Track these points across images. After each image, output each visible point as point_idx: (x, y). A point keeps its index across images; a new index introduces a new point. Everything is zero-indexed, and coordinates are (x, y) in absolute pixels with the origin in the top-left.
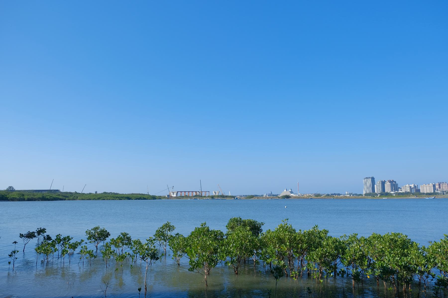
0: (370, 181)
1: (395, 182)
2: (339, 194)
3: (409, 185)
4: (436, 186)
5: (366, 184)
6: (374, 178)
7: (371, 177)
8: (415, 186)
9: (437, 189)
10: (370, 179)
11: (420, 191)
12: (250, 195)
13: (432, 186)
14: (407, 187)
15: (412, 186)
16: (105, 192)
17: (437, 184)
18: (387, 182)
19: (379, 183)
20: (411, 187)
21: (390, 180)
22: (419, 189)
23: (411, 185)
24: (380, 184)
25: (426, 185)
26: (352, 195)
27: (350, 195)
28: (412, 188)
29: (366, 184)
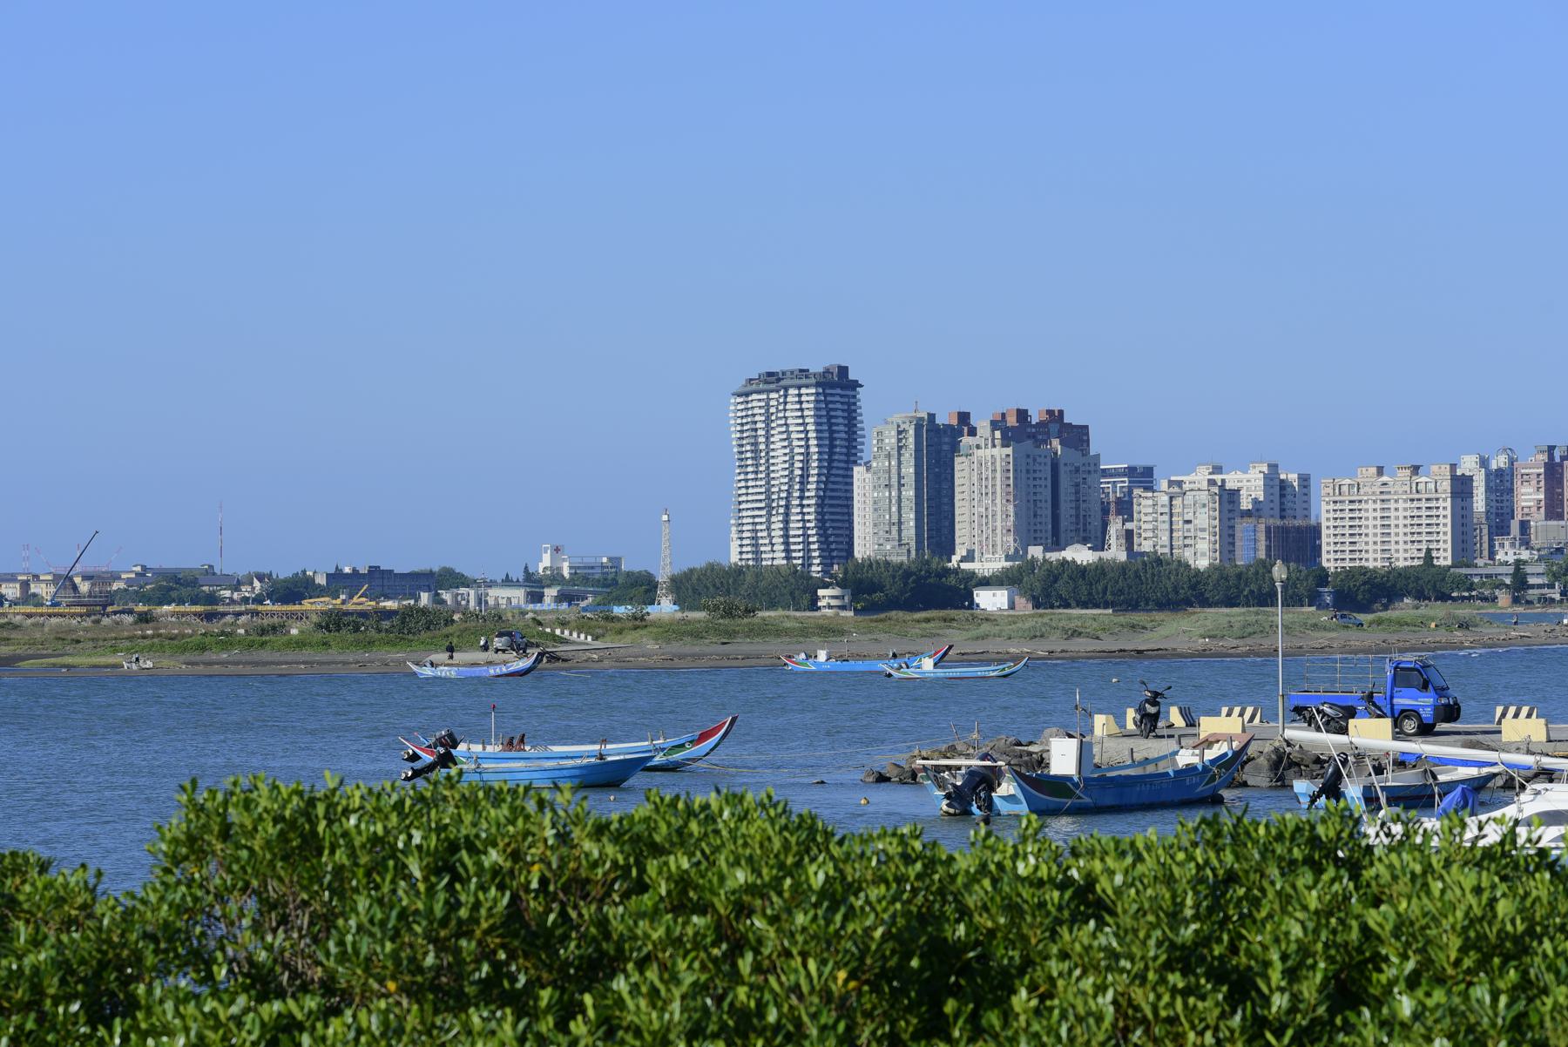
0: (807, 397)
1: (1077, 437)
2: (451, 579)
3: (1218, 478)
4: (1517, 482)
5: (756, 451)
6: (855, 385)
7: (816, 368)
8: (1278, 488)
9: (1524, 526)
10: (809, 393)
11: (1317, 550)
12: (633, 573)
13: (1446, 485)
14: (1189, 498)
15: (1250, 484)
16: (448, 565)
17: (1533, 465)
18: (983, 427)
19: (891, 440)
20: (1229, 498)
21: (1022, 415)
22: (1313, 522)
23: (1232, 480)
24: (908, 457)
25: (1380, 471)
26: (551, 593)
27: (537, 597)
28: (1246, 504)
29: (756, 451)
